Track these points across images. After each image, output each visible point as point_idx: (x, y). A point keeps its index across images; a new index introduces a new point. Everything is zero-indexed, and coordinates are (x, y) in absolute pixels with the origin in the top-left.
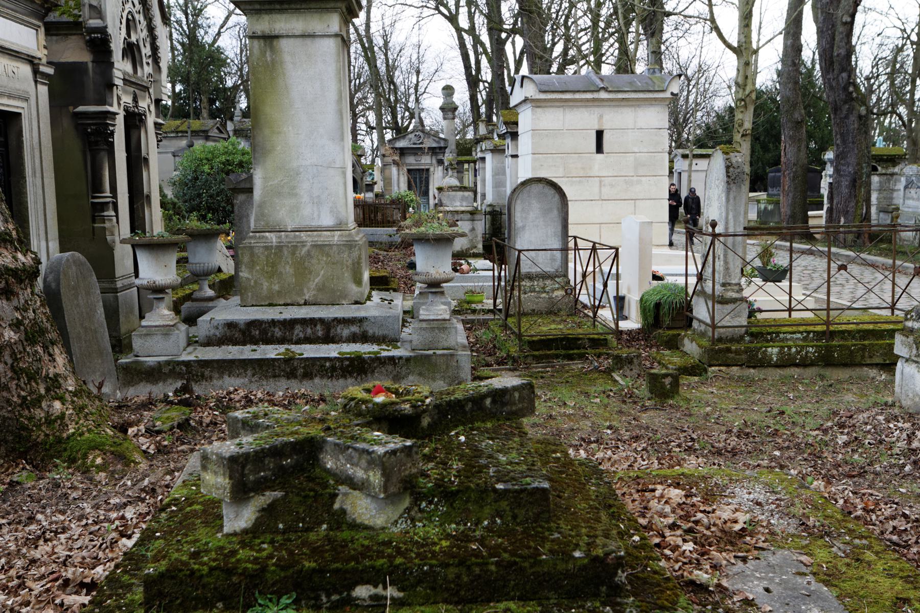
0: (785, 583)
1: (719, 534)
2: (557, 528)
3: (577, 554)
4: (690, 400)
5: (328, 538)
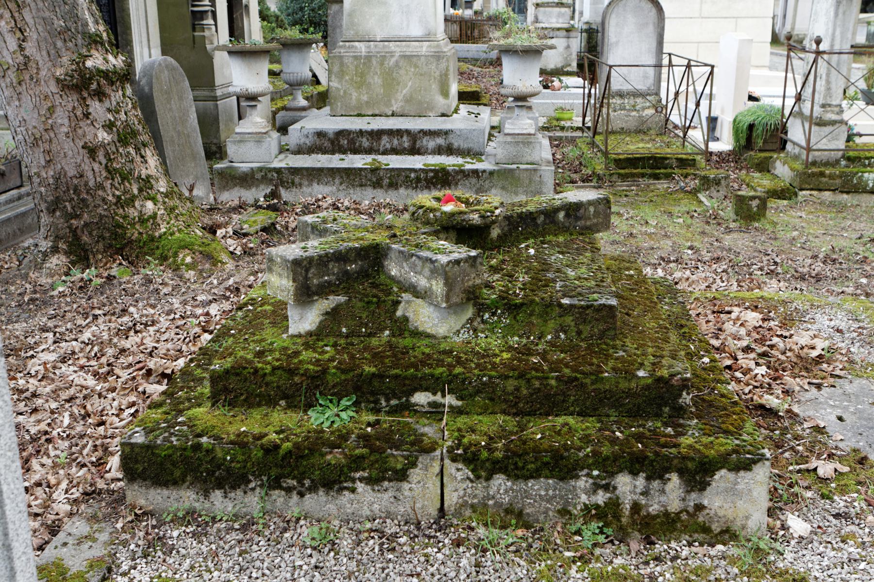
0: (860, 412)
1: (794, 360)
2: (623, 346)
3: (641, 373)
4: (777, 224)
5: (390, 346)
